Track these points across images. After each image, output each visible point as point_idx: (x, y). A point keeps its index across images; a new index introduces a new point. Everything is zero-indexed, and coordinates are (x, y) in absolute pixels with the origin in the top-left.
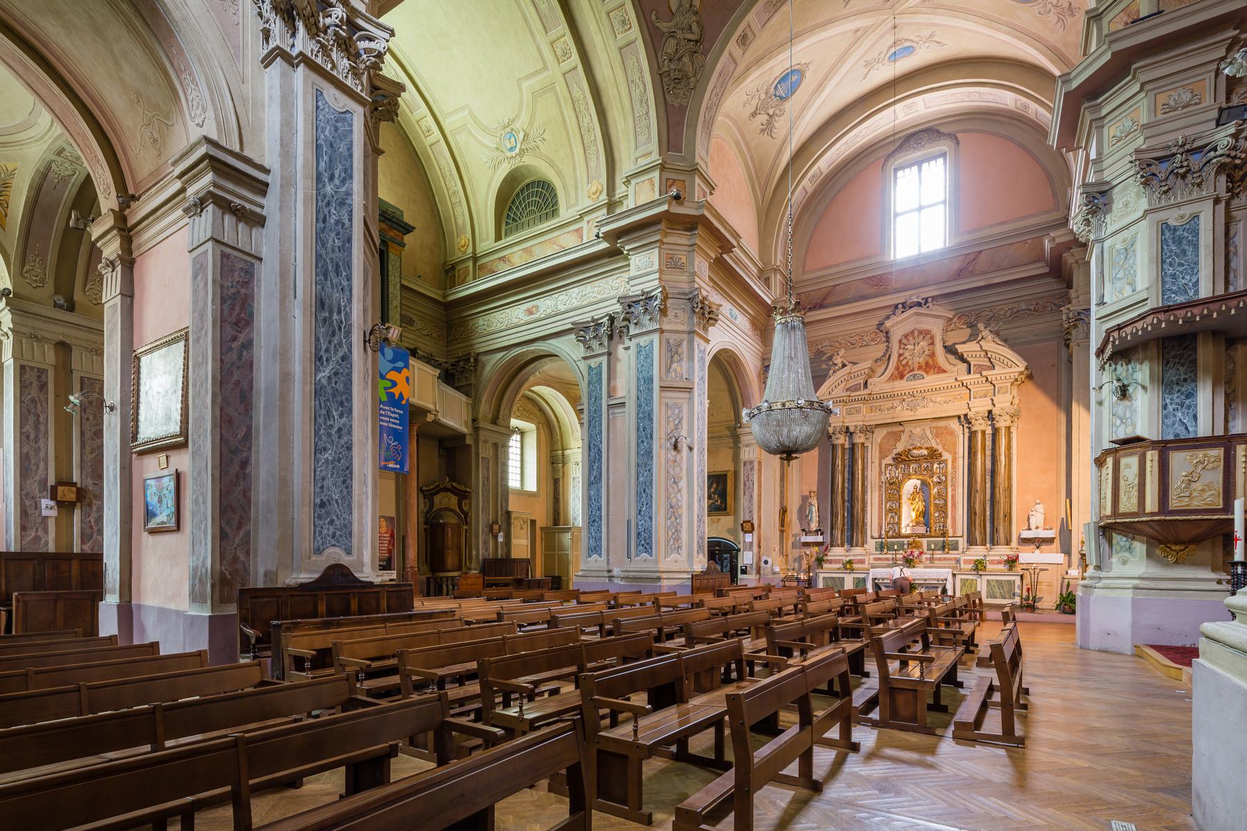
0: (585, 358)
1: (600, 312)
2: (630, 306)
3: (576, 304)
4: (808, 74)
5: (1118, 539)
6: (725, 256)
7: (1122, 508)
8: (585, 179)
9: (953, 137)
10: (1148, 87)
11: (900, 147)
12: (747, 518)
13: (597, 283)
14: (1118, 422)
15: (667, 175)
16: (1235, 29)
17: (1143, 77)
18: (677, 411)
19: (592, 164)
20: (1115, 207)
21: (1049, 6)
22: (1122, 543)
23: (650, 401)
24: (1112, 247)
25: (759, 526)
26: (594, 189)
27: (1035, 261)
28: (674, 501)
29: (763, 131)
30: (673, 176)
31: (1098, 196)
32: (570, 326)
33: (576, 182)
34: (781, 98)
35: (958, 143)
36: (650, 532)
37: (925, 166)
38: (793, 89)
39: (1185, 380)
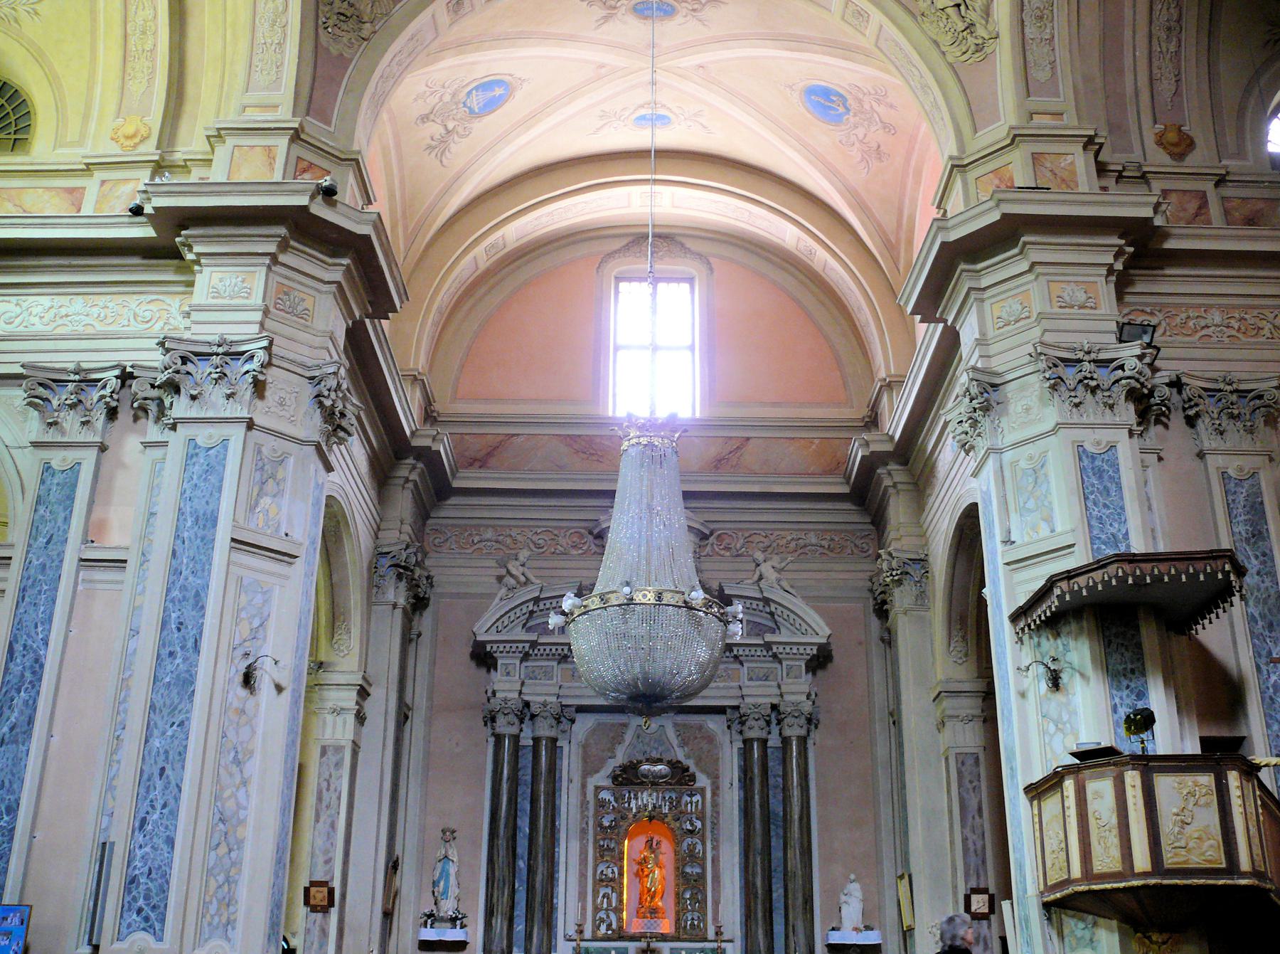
0: (36, 445)
1: (102, 358)
2: (184, 360)
3: (39, 327)
4: (519, 95)
5: (1075, 926)
6: (367, 321)
7: (1098, 867)
8: (112, 108)
9: (699, 256)
10: (1039, 269)
11: (627, 248)
12: (319, 877)
13: (101, 300)
14: (1052, 728)
15: (298, 150)
16: (1120, 237)
17: (1035, 255)
18: (258, 599)
19: (136, 87)
20: (1011, 408)
21: (853, 138)
22: (1079, 933)
23: (202, 567)
24: (1014, 464)
25: (343, 896)
26: (130, 130)
27: (826, 473)
28: (230, 805)
29: (430, 148)
30: (310, 156)
31: (989, 389)
32: (19, 370)
33: (88, 107)
34: (471, 111)
35: (711, 269)
36: (166, 878)
37: (662, 286)
38: (491, 106)
39: (1133, 671)
